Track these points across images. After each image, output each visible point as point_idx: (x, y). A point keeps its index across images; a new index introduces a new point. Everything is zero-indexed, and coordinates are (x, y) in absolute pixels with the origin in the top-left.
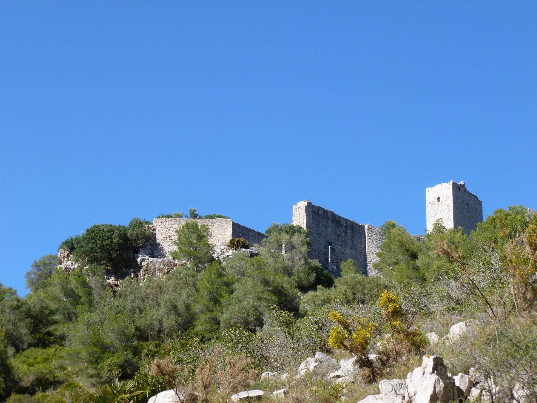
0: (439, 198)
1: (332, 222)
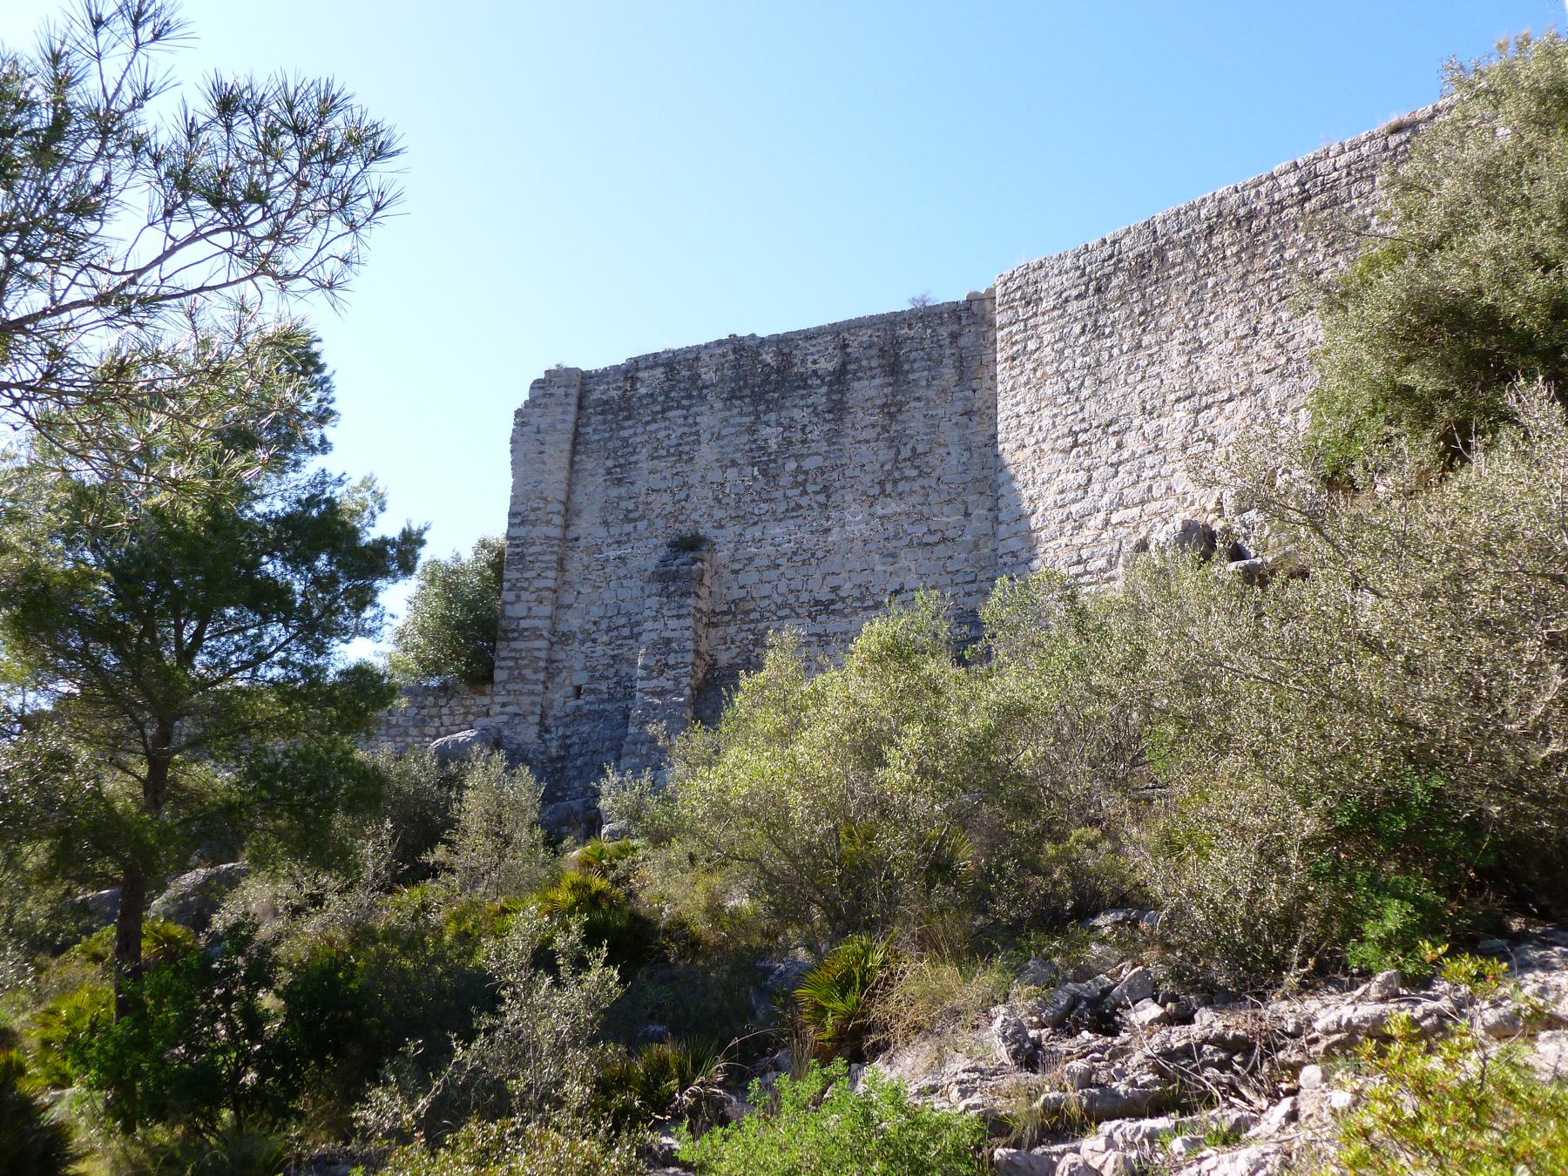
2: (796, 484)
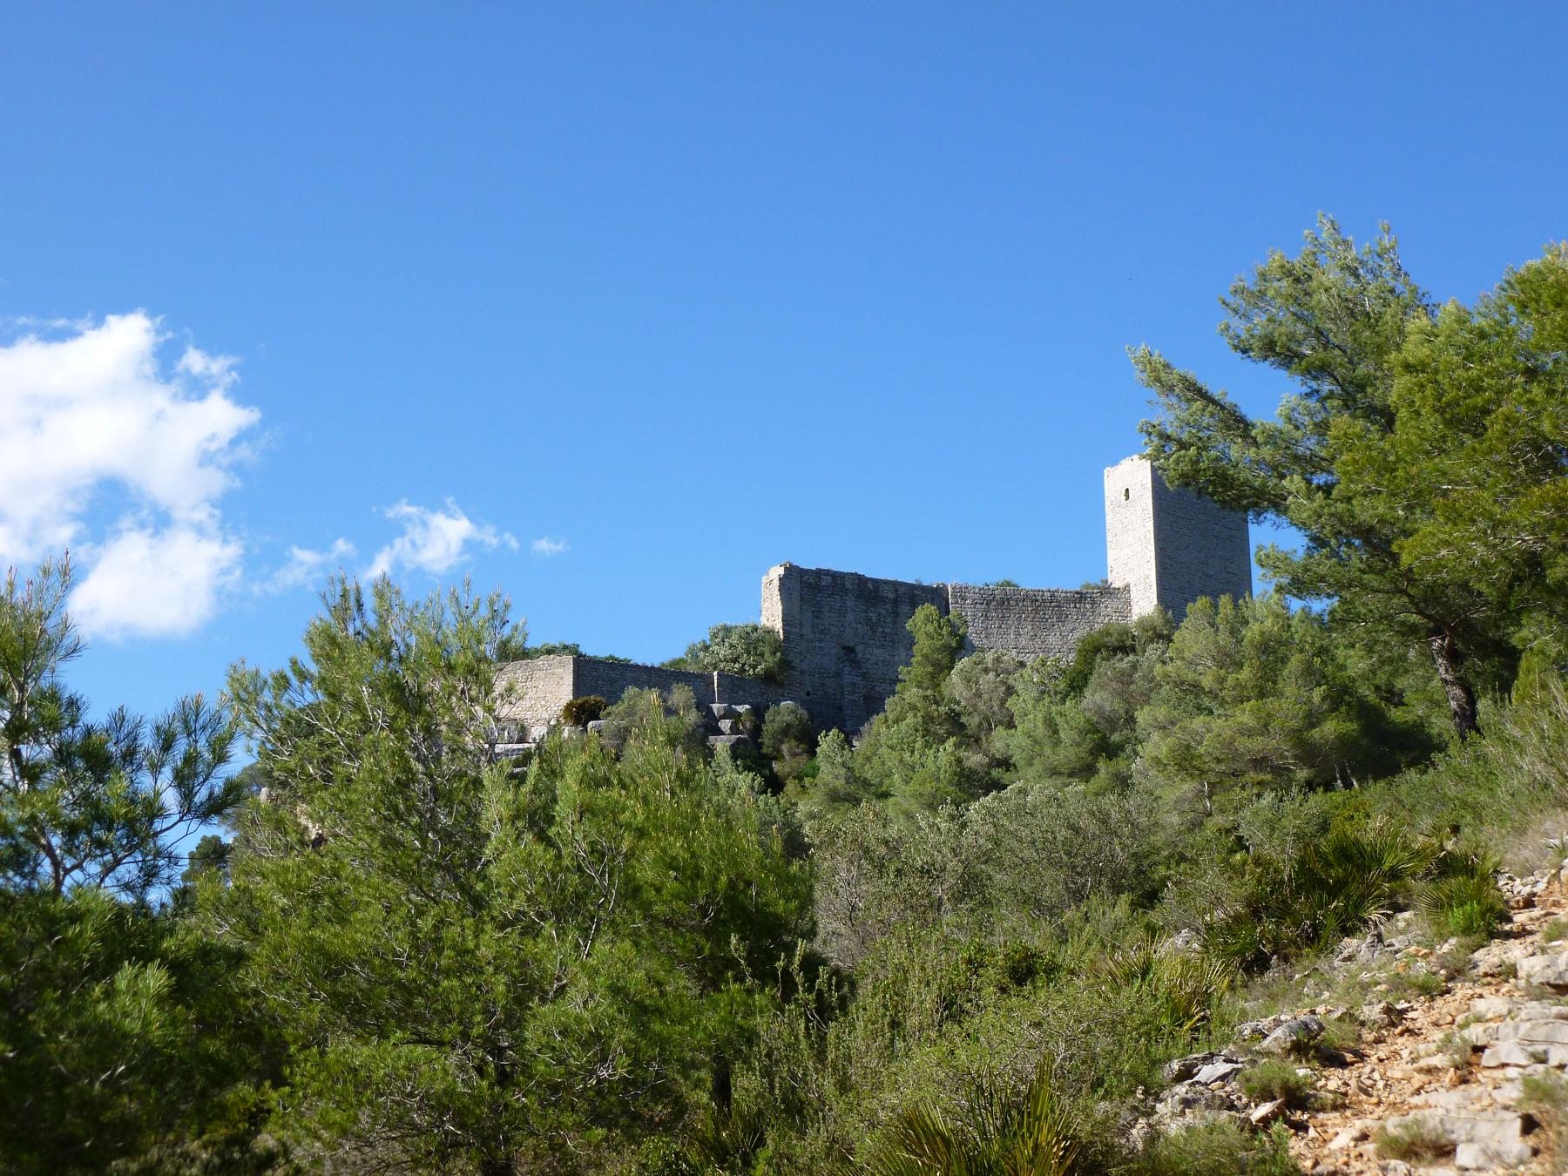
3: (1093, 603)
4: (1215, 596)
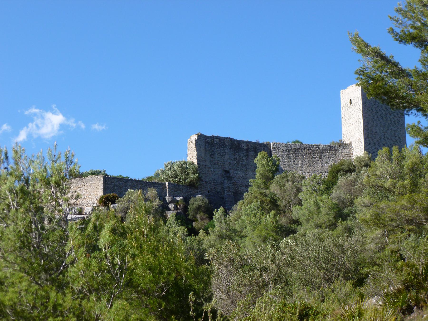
0: (351, 100)
1: (230, 148)
2: (241, 166)
3: (336, 150)
4: (391, 147)
